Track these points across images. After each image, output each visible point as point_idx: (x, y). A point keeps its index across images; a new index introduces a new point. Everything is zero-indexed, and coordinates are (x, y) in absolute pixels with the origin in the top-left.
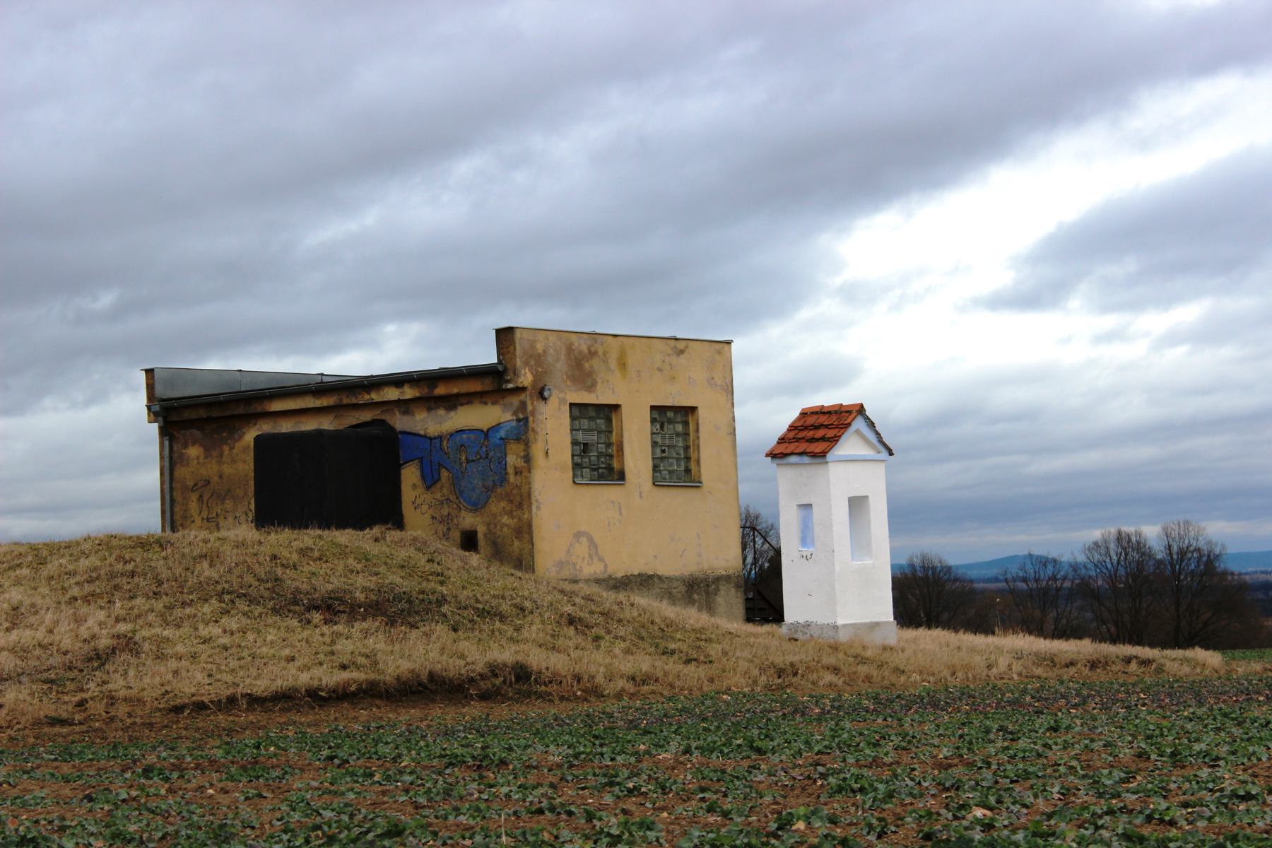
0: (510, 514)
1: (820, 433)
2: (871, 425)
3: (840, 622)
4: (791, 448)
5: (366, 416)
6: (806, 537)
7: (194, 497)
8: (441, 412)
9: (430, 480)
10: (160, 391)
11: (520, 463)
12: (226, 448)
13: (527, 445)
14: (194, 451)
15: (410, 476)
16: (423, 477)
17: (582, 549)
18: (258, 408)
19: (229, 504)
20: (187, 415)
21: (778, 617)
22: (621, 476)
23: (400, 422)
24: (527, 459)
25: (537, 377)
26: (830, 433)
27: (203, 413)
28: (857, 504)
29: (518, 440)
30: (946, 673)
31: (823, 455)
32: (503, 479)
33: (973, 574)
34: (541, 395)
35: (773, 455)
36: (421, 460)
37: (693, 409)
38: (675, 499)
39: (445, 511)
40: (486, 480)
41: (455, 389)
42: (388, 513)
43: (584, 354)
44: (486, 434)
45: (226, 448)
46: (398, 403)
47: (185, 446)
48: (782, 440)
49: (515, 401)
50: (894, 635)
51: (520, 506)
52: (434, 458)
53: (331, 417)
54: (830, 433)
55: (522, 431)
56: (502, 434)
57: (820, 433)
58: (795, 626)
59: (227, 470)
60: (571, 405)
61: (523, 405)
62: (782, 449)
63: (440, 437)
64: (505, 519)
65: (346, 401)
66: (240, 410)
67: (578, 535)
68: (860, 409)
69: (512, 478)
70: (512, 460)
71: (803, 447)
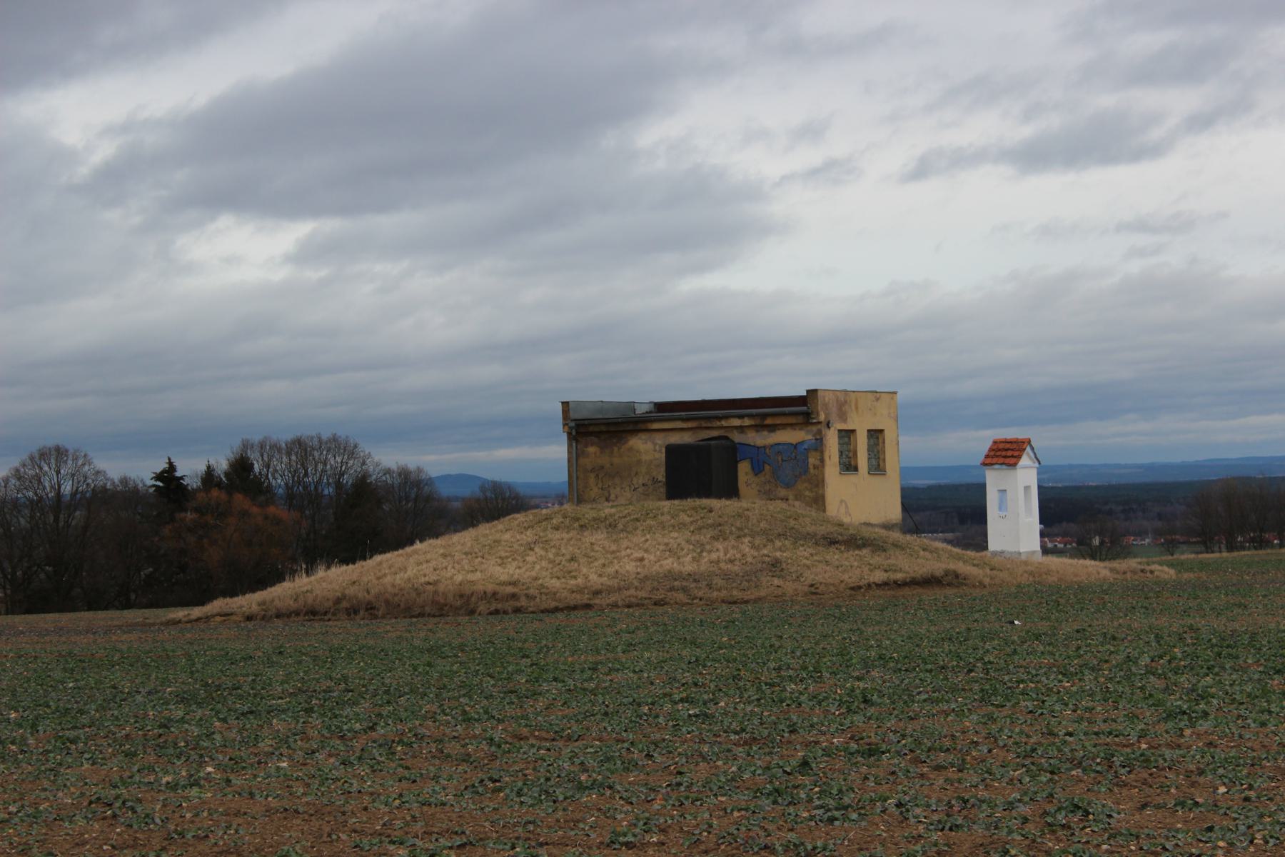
0: (811, 491)
1: (1009, 453)
2: (1032, 449)
3: (1022, 551)
4: (995, 460)
5: (715, 433)
6: (1002, 505)
7: (592, 475)
8: (765, 433)
9: (757, 469)
10: (573, 415)
11: (817, 463)
12: (616, 449)
13: (822, 452)
14: (591, 449)
15: (744, 468)
16: (753, 468)
17: (843, 510)
18: (641, 426)
19: (617, 481)
20: (591, 429)
21: (986, 548)
22: (856, 469)
23: (737, 437)
24: (822, 461)
25: (827, 415)
26: (1016, 454)
27: (603, 428)
28: (1027, 488)
29: (816, 450)
30: (414, 595)
31: (1015, 465)
32: (806, 471)
33: (445, 491)
34: (828, 426)
35: (984, 464)
36: (752, 459)
37: (881, 431)
38: (877, 480)
39: (767, 487)
40: (797, 474)
41: (778, 421)
42: (731, 491)
43: (844, 400)
44: (795, 446)
45: (616, 449)
46: (736, 428)
47: (586, 446)
48: (987, 456)
49: (815, 428)
50: (1039, 557)
51: (817, 486)
52: (759, 459)
53: (690, 433)
54: (1016, 454)
55: (819, 445)
56: (806, 446)
57: (1009, 453)
58: (995, 554)
59: (616, 460)
60: (840, 431)
61: (820, 432)
62: (989, 461)
63: (765, 447)
64: (807, 493)
65: (704, 425)
66: (631, 427)
67: (842, 501)
68: (1029, 442)
69: (812, 471)
70: (812, 461)
71: (1002, 460)
